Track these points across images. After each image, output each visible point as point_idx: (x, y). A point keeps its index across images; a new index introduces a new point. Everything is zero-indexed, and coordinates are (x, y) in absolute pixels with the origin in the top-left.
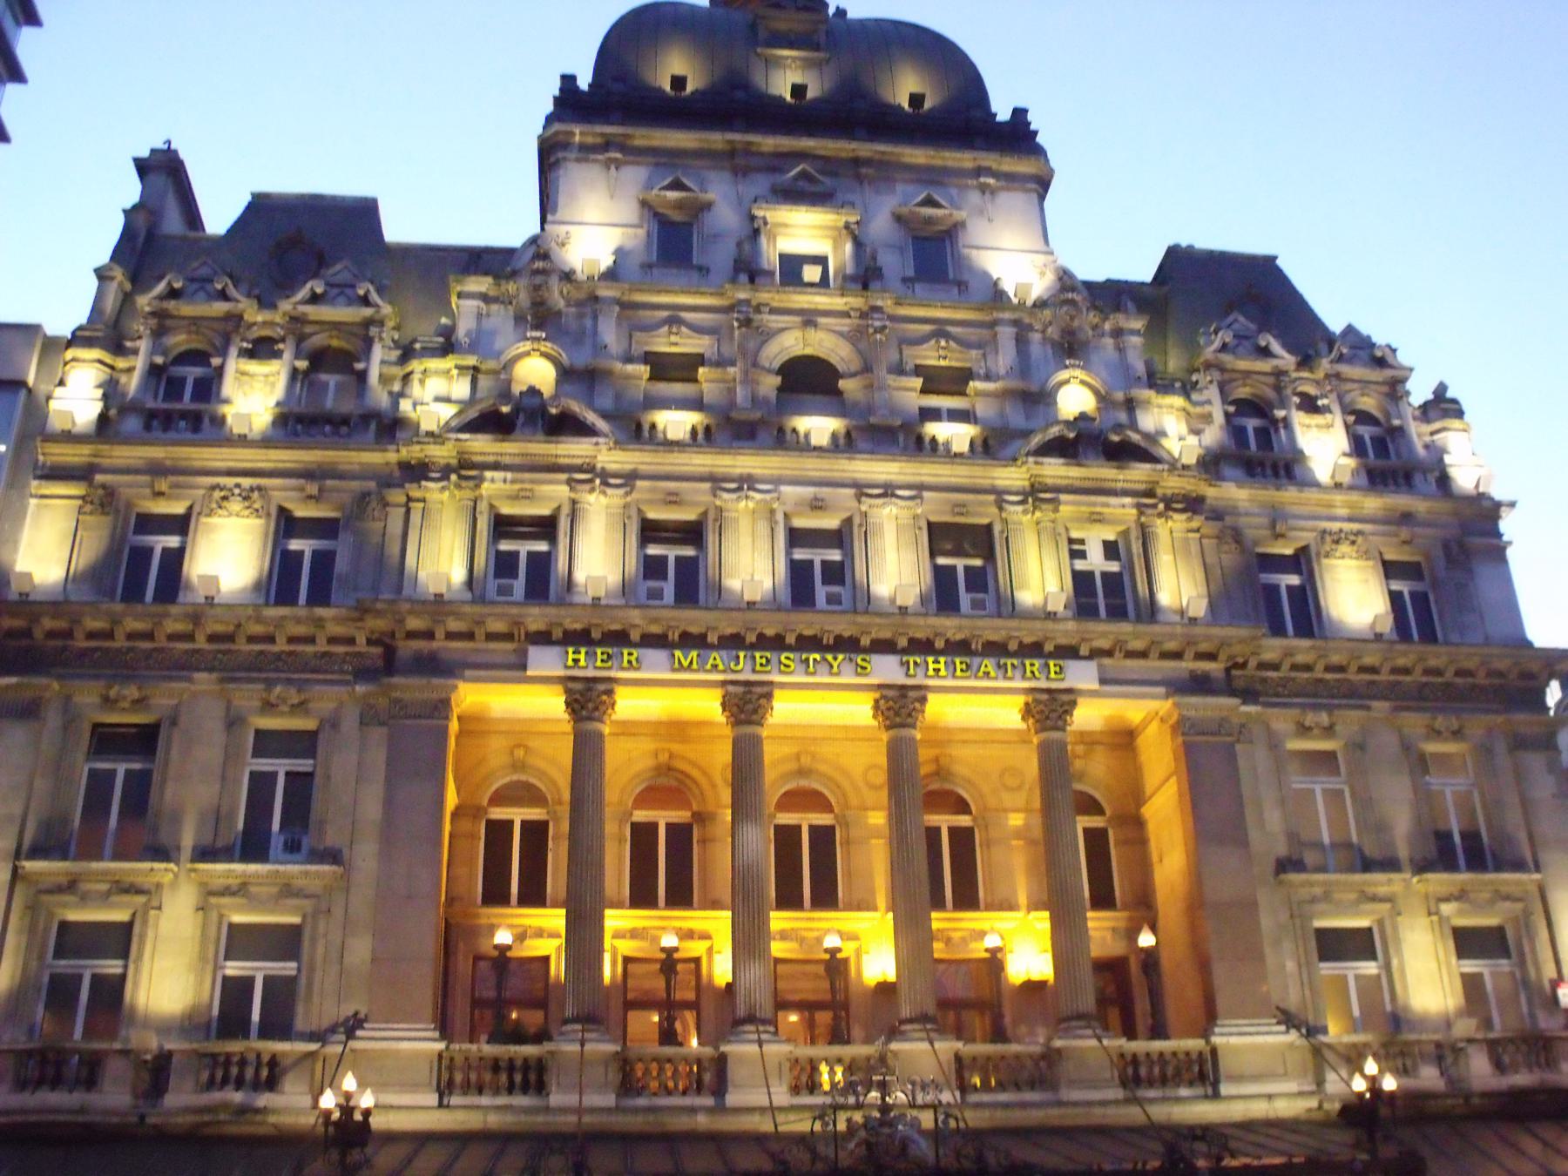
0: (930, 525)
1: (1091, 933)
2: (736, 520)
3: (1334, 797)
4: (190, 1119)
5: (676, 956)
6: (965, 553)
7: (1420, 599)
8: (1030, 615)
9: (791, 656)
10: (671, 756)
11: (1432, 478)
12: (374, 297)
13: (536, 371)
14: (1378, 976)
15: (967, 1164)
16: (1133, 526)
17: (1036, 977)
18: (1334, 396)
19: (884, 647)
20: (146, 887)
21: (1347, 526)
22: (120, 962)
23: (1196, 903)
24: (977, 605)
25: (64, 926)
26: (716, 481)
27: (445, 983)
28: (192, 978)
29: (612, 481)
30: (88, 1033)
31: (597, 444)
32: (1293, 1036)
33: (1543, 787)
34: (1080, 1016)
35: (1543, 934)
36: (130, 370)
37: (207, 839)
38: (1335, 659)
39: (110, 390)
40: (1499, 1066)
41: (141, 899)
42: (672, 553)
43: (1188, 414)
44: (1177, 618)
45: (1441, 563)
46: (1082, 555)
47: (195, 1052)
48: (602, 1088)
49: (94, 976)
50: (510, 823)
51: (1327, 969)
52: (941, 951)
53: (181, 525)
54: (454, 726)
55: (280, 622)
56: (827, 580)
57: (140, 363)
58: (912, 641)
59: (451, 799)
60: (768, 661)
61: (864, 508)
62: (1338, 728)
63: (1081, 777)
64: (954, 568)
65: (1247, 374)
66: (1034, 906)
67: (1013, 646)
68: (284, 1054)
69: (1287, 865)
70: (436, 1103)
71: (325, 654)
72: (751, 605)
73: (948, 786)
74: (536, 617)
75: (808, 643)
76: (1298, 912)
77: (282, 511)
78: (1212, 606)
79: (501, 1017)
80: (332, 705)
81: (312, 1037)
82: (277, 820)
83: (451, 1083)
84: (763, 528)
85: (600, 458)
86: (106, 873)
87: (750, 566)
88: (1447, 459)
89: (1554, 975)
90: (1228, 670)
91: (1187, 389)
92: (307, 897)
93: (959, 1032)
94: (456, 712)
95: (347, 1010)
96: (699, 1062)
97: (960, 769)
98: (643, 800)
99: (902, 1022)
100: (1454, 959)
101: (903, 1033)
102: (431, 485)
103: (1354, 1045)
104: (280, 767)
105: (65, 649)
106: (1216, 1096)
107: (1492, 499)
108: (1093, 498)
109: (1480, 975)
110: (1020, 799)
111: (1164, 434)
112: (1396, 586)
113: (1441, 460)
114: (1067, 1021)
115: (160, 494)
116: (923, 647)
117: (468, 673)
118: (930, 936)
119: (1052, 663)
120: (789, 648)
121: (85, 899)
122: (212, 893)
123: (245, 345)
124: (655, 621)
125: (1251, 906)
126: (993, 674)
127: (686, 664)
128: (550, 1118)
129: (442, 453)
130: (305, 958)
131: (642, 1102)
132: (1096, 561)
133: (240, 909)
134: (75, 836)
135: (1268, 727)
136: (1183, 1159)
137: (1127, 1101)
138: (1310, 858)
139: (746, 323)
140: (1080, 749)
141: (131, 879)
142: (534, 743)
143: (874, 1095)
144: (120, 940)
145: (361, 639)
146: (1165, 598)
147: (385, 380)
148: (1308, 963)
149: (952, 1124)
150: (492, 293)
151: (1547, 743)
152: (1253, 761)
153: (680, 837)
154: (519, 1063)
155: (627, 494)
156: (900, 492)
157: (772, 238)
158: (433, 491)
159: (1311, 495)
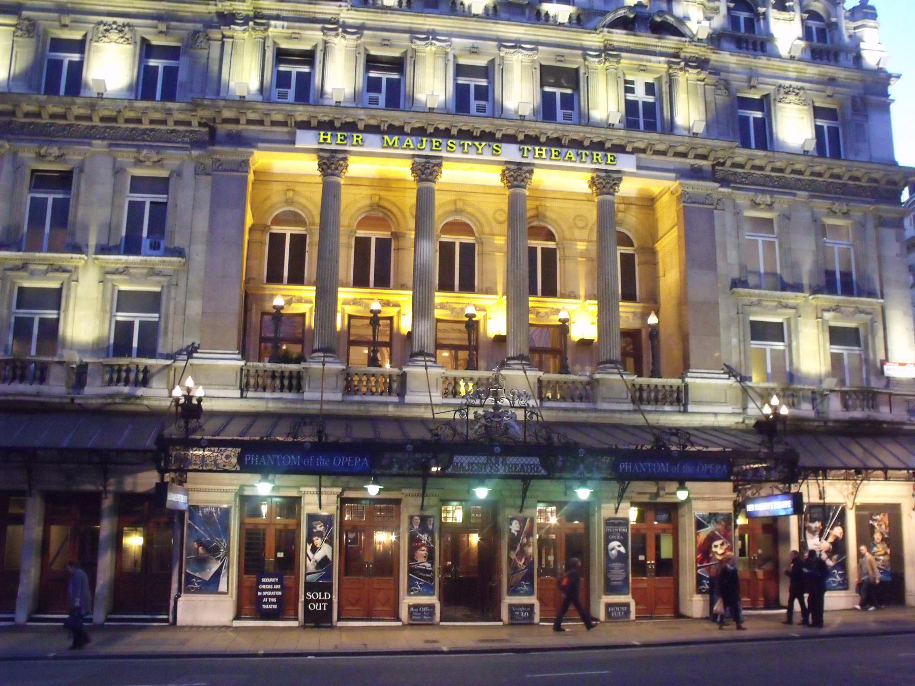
0: (541, 66)
1: (621, 314)
2: (424, 57)
3: (769, 245)
4: (100, 401)
5: (379, 315)
6: (562, 85)
7: (834, 132)
8: (597, 125)
9: (454, 142)
11: (851, 56)
14: (784, 350)
15: (542, 441)
16: (664, 74)
17: (587, 337)
19: (510, 139)
20: (69, 268)
21: (795, 84)
22: (55, 312)
23: (683, 301)
24: (567, 117)
25: (21, 290)
26: (413, 33)
27: (245, 329)
28: (98, 322)
30: (39, 351)
31: (340, 6)
32: (732, 381)
33: (892, 248)
34: (611, 362)
35: (880, 334)
37: (104, 241)
38: (778, 164)
40: (846, 406)
41: (66, 275)
42: (385, 76)
43: (705, 6)
44: (686, 133)
45: (849, 111)
47: (101, 363)
48: (334, 389)
50: (284, 235)
51: (755, 344)
52: (533, 319)
53: (80, 46)
54: (251, 177)
55: (145, 111)
56: (477, 98)
59: (249, 221)
60: (440, 144)
61: (502, 54)
62: (775, 205)
63: (621, 224)
64: (554, 93)
66: (589, 297)
67: (587, 143)
68: (152, 366)
69: (737, 283)
70: (239, 396)
71: (173, 131)
72: (431, 110)
73: (542, 224)
74: (302, 112)
75: (465, 135)
76: (741, 311)
77: (144, 40)
78: (708, 126)
79: (277, 347)
80: (177, 162)
81: (168, 356)
82: (146, 230)
83: (247, 384)
84: (440, 63)
85: (342, 15)
86: (45, 259)
87: (431, 86)
88: (862, 45)
89: (884, 358)
90: (713, 166)
92: (164, 276)
93: (540, 367)
94: (252, 168)
95: (188, 342)
96: (390, 376)
97: (549, 214)
98: (361, 224)
99: (509, 359)
100: (828, 345)
101: (508, 365)
102: (237, 28)
103: (766, 389)
104: (148, 199)
106: (685, 411)
107: (886, 72)
108: (641, 56)
109: (842, 354)
110: (584, 234)
111: (688, 19)
112: (820, 122)
113: (858, 45)
114: (603, 363)
115: (65, 26)
116: (532, 140)
117: (260, 145)
118: (528, 311)
119: (609, 155)
120: (453, 137)
121: (33, 274)
122: (107, 273)
124: (373, 117)
125: (714, 306)
126: (573, 159)
127: (391, 144)
128: (304, 406)
130: (163, 309)
131: (357, 398)
132: (640, 95)
133: (125, 282)
134: (25, 238)
135: (734, 201)
136: (664, 445)
137: (635, 411)
138: (752, 280)
140: (622, 207)
141: (60, 263)
142: (299, 188)
143: (490, 400)
144: (55, 298)
145: (195, 123)
148: (744, 340)
149: (535, 418)
151: (898, 224)
152: (724, 220)
153: (384, 246)
154: (287, 374)
155: (359, 38)
156: (523, 46)
158: (238, 31)
159: (775, 63)
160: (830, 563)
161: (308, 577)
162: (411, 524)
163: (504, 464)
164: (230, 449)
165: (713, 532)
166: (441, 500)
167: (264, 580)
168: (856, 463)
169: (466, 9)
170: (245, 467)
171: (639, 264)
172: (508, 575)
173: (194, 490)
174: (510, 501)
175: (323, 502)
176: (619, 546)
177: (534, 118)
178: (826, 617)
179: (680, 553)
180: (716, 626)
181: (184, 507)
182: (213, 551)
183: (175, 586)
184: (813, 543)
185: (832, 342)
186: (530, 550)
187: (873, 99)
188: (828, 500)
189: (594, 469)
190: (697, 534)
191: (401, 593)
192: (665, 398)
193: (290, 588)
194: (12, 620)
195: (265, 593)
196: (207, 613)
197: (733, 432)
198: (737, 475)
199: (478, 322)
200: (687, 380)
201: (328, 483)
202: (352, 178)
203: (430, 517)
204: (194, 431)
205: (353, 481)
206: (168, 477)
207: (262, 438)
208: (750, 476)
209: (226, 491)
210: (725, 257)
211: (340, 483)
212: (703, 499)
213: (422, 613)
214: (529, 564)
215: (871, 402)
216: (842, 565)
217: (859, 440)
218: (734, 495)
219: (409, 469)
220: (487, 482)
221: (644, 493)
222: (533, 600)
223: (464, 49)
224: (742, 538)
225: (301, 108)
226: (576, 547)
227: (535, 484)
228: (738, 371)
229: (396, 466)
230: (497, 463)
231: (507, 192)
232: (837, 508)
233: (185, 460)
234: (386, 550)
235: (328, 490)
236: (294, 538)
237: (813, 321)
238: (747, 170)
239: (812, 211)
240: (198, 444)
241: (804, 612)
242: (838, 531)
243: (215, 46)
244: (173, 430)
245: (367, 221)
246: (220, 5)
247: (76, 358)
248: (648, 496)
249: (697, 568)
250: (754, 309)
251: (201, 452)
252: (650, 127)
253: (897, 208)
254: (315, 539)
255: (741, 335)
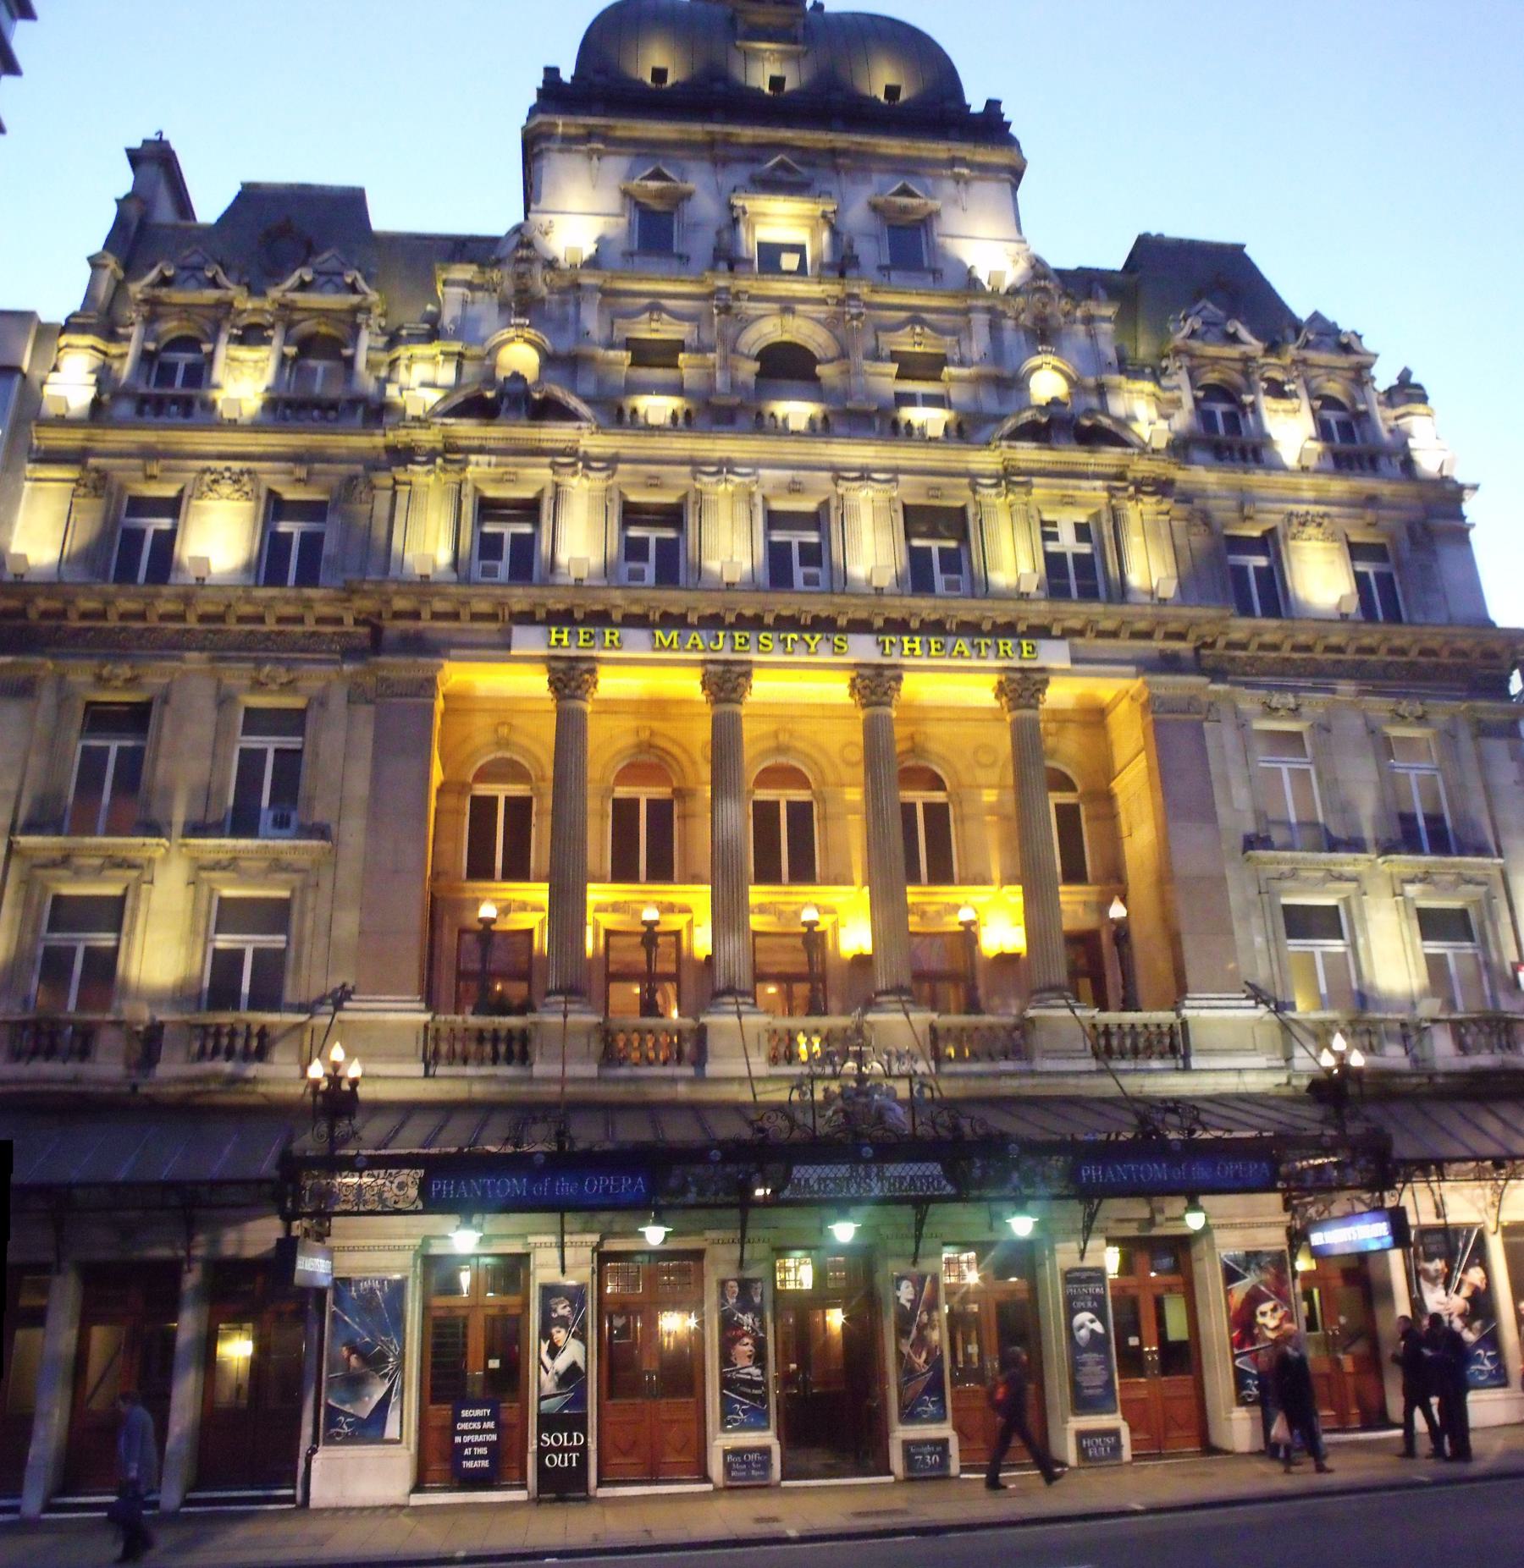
0: (905, 507)
1: (1063, 907)
2: (716, 503)
3: (1301, 776)
4: (182, 1088)
5: (657, 929)
6: (939, 535)
7: (1385, 581)
8: (1003, 596)
10: (652, 733)
11: (1396, 461)
12: (362, 284)
13: (520, 357)
15: (943, 1132)
17: (1009, 950)
18: (1300, 381)
19: (861, 626)
20: (138, 861)
21: (1314, 509)
22: (112, 935)
23: (1165, 877)
24: (952, 586)
25: (58, 900)
26: (696, 464)
27: (431, 955)
28: (183, 951)
29: (594, 465)
30: (82, 1004)
32: (1262, 1011)
34: (1053, 988)
35: (1505, 918)
36: (123, 356)
37: (198, 815)
38: (1302, 638)
39: (103, 376)
40: (1462, 1047)
41: (134, 873)
42: (653, 535)
44: (1147, 599)
46: (1054, 537)
48: (584, 1058)
49: (88, 950)
50: (495, 798)
51: (1295, 945)
52: (916, 924)
53: (172, 507)
54: (440, 704)
55: (269, 603)
57: (132, 349)
58: (887, 621)
59: (437, 776)
60: (747, 640)
61: (840, 491)
62: (1303, 710)
63: (1053, 753)
64: (929, 549)
65: (1216, 360)
66: (1007, 880)
67: (987, 626)
68: (273, 1025)
70: (422, 1073)
71: (313, 634)
72: (730, 586)
73: (922, 763)
74: (520, 597)
76: (1266, 890)
77: (271, 493)
79: (486, 989)
80: (319, 684)
81: (301, 1008)
82: (265, 796)
83: (436, 1053)
84: (742, 510)
85: (582, 442)
86: (99, 848)
87: (729, 548)
88: (1412, 443)
89: (1516, 959)
90: (1197, 650)
91: (1157, 375)
93: (934, 1004)
94: (441, 690)
95: (336, 982)
96: (679, 1032)
97: (934, 747)
98: (625, 776)
99: (879, 994)
100: (1418, 940)
102: (417, 468)
103: (1322, 1023)
104: (270, 744)
105: (58, 628)
106: (1187, 1069)
107: (1455, 482)
108: (1065, 482)
109: (1444, 956)
110: (993, 776)
111: (1134, 418)
112: (1361, 567)
113: (1406, 444)
116: (899, 627)
117: (453, 652)
118: (906, 910)
119: (1024, 643)
120: (768, 628)
121: (78, 874)
122: (203, 868)
123: (235, 331)
124: (636, 601)
126: (967, 653)
127: (666, 643)
128: (534, 1088)
129: (428, 438)
131: (623, 1072)
132: (1068, 543)
133: (231, 883)
134: (69, 812)
136: (1156, 1131)
137: (1100, 1072)
138: (1278, 835)
139: (726, 310)
140: (1052, 727)
141: (124, 854)
142: (517, 721)
143: (851, 1065)
144: (113, 914)
145: (349, 620)
146: (1135, 579)
147: (371, 365)
148: (1276, 940)
149: (927, 1093)
150: (476, 281)
152: (1221, 738)
153: (661, 812)
154: (503, 1034)
155: (609, 477)
156: (876, 476)
157: (751, 227)
158: (419, 474)
159: (1279, 478)
160: (1469, 1336)
161: (544, 1404)
162: (723, 1296)
163: (881, 1178)
164: (406, 1171)
165: (1255, 1288)
166: (773, 1249)
167: (465, 1413)
168: (1492, 1149)
169: (780, 423)
170: (431, 1203)
171: (1088, 818)
172: (899, 1386)
173: (343, 1249)
174: (894, 1245)
175: (567, 1262)
176: (1092, 1321)
177: (899, 591)
178: (1475, 1441)
179: (1202, 1330)
180: (1278, 1468)
181: (325, 1282)
182: (374, 1361)
183: (307, 1431)
184: (1436, 1299)
185: (1425, 936)
186: (935, 1336)
187: (1440, 524)
188: (1452, 1218)
189: (1038, 1179)
190: (1228, 1293)
191: (710, 1428)
192: (1149, 1046)
193: (512, 1426)
194: (15, 1509)
195: (467, 1439)
196: (362, 1477)
197: (1273, 1103)
198: (1286, 1179)
199: (823, 934)
200: (1186, 1013)
201: (578, 1227)
202: (606, 701)
203: (755, 1280)
204: (345, 1142)
205: (619, 1221)
206: (297, 1227)
207: (460, 1149)
208: (1310, 1180)
209: (399, 1249)
210: (1229, 800)
211: (596, 1226)
212: (1232, 1225)
213: (748, 1464)
214: (935, 1363)
215: (1504, 1038)
216: (1492, 1339)
217: (1492, 1106)
218: (1287, 1217)
219: (716, 1194)
220: (853, 1211)
221: (1129, 1220)
222: (945, 1430)
223: (777, 486)
224: (1308, 1296)
225: (519, 591)
226: (1016, 1326)
227: (936, 1212)
228: (1271, 993)
229: (694, 1189)
230: (868, 1176)
231: (861, 714)
232: (1470, 1232)
233: (328, 1195)
234: (680, 1345)
235: (576, 1238)
236: (518, 1330)
237: (1389, 901)
238: (1252, 651)
239: (1366, 717)
240: (351, 1165)
241: (1435, 1432)
242: (1476, 1276)
243: (383, 498)
244: (309, 1142)
245: (633, 771)
246: (391, 436)
247: (144, 1014)
248: (1135, 1225)
249: (1235, 1357)
250: (1288, 884)
251: (356, 1180)
252: (1089, 593)
253: (1505, 705)
254: (554, 1330)
255: (1270, 929)
